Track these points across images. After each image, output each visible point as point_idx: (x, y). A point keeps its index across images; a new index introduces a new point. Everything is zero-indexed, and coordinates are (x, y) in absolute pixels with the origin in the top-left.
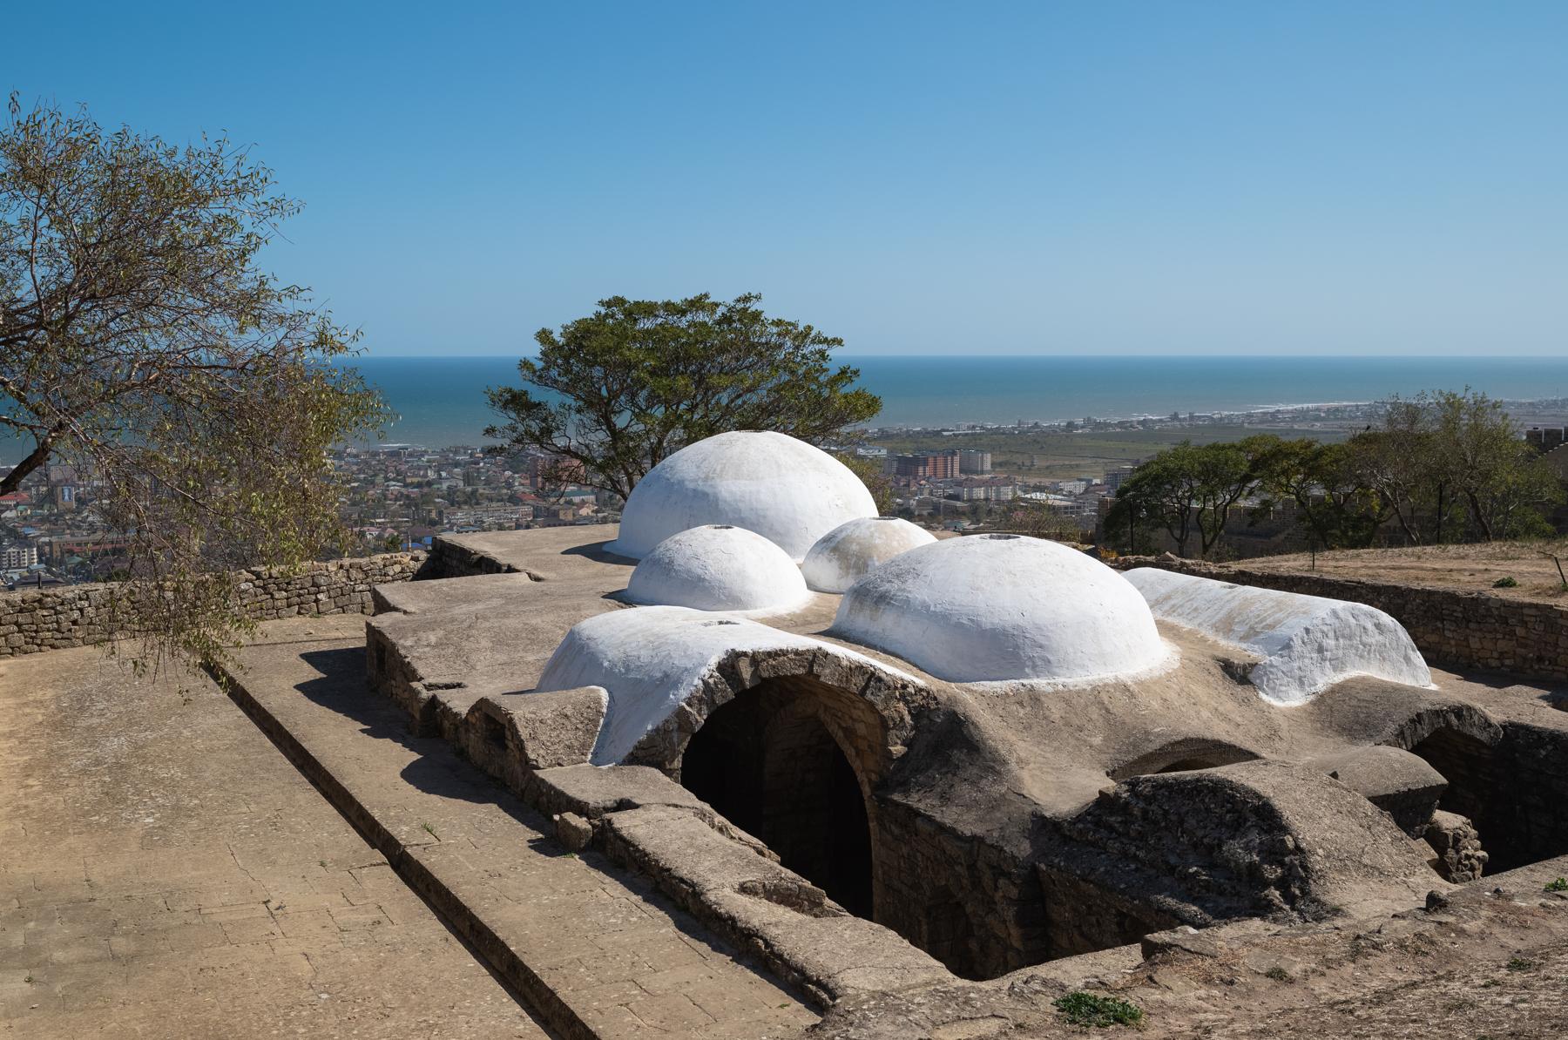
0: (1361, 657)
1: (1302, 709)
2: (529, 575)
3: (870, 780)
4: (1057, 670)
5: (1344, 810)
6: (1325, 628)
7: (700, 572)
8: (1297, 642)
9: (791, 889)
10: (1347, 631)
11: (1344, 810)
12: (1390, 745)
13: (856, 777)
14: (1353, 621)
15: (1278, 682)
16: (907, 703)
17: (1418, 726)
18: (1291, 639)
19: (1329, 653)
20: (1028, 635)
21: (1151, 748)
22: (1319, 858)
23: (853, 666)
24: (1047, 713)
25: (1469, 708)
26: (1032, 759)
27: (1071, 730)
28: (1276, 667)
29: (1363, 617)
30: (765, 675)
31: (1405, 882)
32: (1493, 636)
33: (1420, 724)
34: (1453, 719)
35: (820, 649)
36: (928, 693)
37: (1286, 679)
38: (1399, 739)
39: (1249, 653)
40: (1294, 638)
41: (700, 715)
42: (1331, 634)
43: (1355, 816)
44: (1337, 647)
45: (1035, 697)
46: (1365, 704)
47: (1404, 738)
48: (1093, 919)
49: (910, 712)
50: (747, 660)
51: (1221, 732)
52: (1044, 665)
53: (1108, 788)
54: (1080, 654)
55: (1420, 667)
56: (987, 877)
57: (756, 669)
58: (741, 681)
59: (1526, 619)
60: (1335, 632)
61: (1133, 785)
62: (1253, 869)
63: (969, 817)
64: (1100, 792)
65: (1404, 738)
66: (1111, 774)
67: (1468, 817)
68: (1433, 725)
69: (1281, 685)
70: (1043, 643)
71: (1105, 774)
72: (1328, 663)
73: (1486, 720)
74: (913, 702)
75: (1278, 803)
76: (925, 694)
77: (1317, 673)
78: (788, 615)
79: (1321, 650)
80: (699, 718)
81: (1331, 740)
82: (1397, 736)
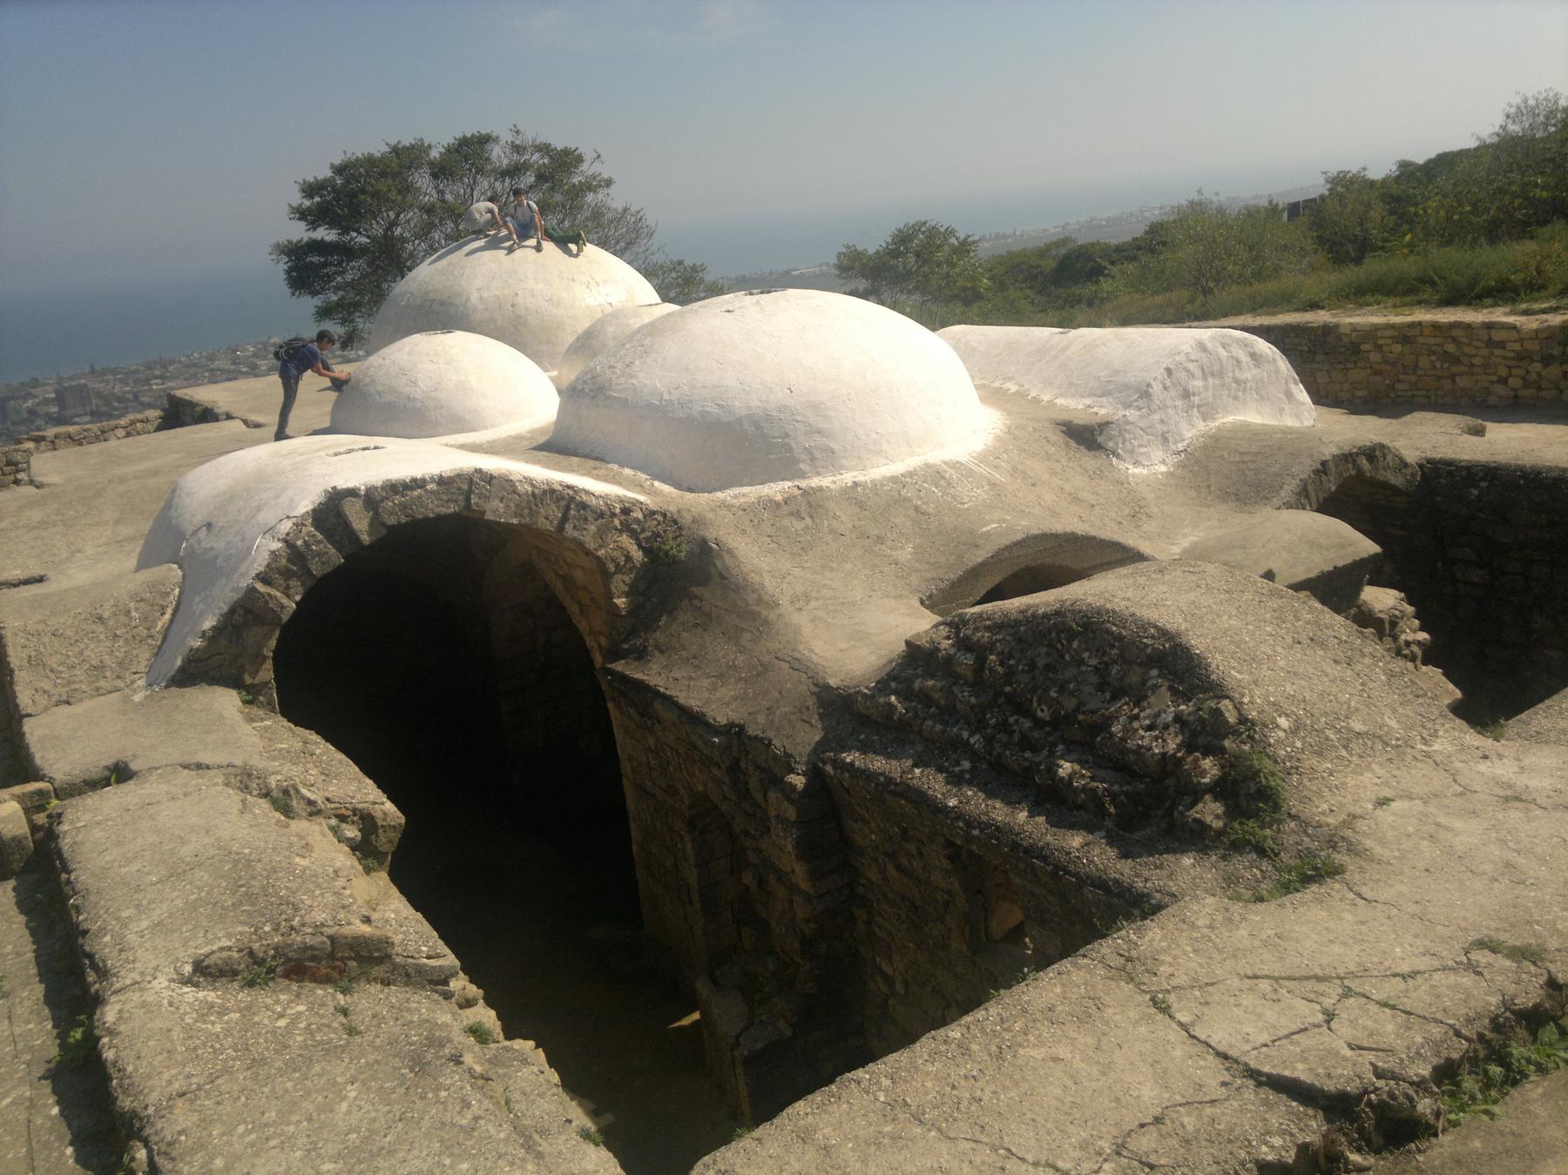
0: (1236, 398)
1: (1169, 474)
2: (245, 422)
3: (600, 646)
4: (844, 462)
5: (1303, 638)
6: (1191, 366)
7: (407, 390)
8: (1156, 388)
9: (312, 948)
10: (1216, 368)
11: (1303, 638)
12: (1291, 507)
13: (584, 642)
14: (1223, 353)
15: (1136, 443)
16: (634, 535)
17: (1324, 477)
18: (1149, 385)
19: (1197, 398)
20: (799, 418)
21: (980, 556)
22: (1281, 734)
23: (536, 491)
24: (835, 524)
25: (1382, 447)
26: (814, 594)
27: (866, 543)
28: (1133, 423)
29: (1235, 345)
30: (392, 521)
31: (1428, 755)
32: (1343, 367)
33: (1326, 474)
34: (1364, 464)
35: (478, 471)
36: (664, 515)
37: (1146, 437)
38: (1304, 498)
39: (1095, 410)
40: (1153, 383)
41: (288, 596)
42: (1198, 373)
43: (1323, 645)
44: (1206, 388)
45: (812, 503)
46: (1249, 458)
47: (1307, 496)
48: (912, 848)
49: (640, 546)
50: (359, 503)
51: (1070, 522)
52: (828, 459)
53: (918, 635)
54: (875, 436)
55: (1303, 404)
56: (754, 784)
57: (377, 514)
58: (352, 534)
59: (1380, 342)
60: (1203, 370)
61: (956, 626)
62: (1169, 764)
63: (727, 692)
64: (908, 643)
65: (1307, 496)
66: (930, 603)
67: (1401, 591)
68: (1341, 474)
69: (1140, 446)
70: (820, 425)
71: (917, 604)
72: (1195, 410)
73: (1401, 459)
74: (643, 531)
75: (1198, 643)
76: (660, 518)
77: (1184, 425)
78: (528, 432)
79: (1186, 395)
80: (287, 603)
81: (1212, 509)
82: (1299, 494)
